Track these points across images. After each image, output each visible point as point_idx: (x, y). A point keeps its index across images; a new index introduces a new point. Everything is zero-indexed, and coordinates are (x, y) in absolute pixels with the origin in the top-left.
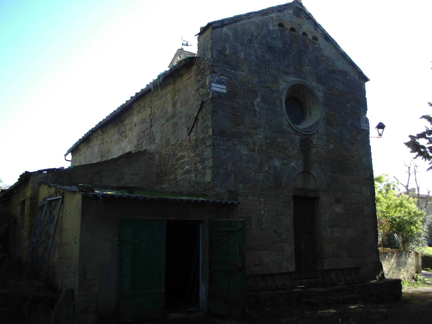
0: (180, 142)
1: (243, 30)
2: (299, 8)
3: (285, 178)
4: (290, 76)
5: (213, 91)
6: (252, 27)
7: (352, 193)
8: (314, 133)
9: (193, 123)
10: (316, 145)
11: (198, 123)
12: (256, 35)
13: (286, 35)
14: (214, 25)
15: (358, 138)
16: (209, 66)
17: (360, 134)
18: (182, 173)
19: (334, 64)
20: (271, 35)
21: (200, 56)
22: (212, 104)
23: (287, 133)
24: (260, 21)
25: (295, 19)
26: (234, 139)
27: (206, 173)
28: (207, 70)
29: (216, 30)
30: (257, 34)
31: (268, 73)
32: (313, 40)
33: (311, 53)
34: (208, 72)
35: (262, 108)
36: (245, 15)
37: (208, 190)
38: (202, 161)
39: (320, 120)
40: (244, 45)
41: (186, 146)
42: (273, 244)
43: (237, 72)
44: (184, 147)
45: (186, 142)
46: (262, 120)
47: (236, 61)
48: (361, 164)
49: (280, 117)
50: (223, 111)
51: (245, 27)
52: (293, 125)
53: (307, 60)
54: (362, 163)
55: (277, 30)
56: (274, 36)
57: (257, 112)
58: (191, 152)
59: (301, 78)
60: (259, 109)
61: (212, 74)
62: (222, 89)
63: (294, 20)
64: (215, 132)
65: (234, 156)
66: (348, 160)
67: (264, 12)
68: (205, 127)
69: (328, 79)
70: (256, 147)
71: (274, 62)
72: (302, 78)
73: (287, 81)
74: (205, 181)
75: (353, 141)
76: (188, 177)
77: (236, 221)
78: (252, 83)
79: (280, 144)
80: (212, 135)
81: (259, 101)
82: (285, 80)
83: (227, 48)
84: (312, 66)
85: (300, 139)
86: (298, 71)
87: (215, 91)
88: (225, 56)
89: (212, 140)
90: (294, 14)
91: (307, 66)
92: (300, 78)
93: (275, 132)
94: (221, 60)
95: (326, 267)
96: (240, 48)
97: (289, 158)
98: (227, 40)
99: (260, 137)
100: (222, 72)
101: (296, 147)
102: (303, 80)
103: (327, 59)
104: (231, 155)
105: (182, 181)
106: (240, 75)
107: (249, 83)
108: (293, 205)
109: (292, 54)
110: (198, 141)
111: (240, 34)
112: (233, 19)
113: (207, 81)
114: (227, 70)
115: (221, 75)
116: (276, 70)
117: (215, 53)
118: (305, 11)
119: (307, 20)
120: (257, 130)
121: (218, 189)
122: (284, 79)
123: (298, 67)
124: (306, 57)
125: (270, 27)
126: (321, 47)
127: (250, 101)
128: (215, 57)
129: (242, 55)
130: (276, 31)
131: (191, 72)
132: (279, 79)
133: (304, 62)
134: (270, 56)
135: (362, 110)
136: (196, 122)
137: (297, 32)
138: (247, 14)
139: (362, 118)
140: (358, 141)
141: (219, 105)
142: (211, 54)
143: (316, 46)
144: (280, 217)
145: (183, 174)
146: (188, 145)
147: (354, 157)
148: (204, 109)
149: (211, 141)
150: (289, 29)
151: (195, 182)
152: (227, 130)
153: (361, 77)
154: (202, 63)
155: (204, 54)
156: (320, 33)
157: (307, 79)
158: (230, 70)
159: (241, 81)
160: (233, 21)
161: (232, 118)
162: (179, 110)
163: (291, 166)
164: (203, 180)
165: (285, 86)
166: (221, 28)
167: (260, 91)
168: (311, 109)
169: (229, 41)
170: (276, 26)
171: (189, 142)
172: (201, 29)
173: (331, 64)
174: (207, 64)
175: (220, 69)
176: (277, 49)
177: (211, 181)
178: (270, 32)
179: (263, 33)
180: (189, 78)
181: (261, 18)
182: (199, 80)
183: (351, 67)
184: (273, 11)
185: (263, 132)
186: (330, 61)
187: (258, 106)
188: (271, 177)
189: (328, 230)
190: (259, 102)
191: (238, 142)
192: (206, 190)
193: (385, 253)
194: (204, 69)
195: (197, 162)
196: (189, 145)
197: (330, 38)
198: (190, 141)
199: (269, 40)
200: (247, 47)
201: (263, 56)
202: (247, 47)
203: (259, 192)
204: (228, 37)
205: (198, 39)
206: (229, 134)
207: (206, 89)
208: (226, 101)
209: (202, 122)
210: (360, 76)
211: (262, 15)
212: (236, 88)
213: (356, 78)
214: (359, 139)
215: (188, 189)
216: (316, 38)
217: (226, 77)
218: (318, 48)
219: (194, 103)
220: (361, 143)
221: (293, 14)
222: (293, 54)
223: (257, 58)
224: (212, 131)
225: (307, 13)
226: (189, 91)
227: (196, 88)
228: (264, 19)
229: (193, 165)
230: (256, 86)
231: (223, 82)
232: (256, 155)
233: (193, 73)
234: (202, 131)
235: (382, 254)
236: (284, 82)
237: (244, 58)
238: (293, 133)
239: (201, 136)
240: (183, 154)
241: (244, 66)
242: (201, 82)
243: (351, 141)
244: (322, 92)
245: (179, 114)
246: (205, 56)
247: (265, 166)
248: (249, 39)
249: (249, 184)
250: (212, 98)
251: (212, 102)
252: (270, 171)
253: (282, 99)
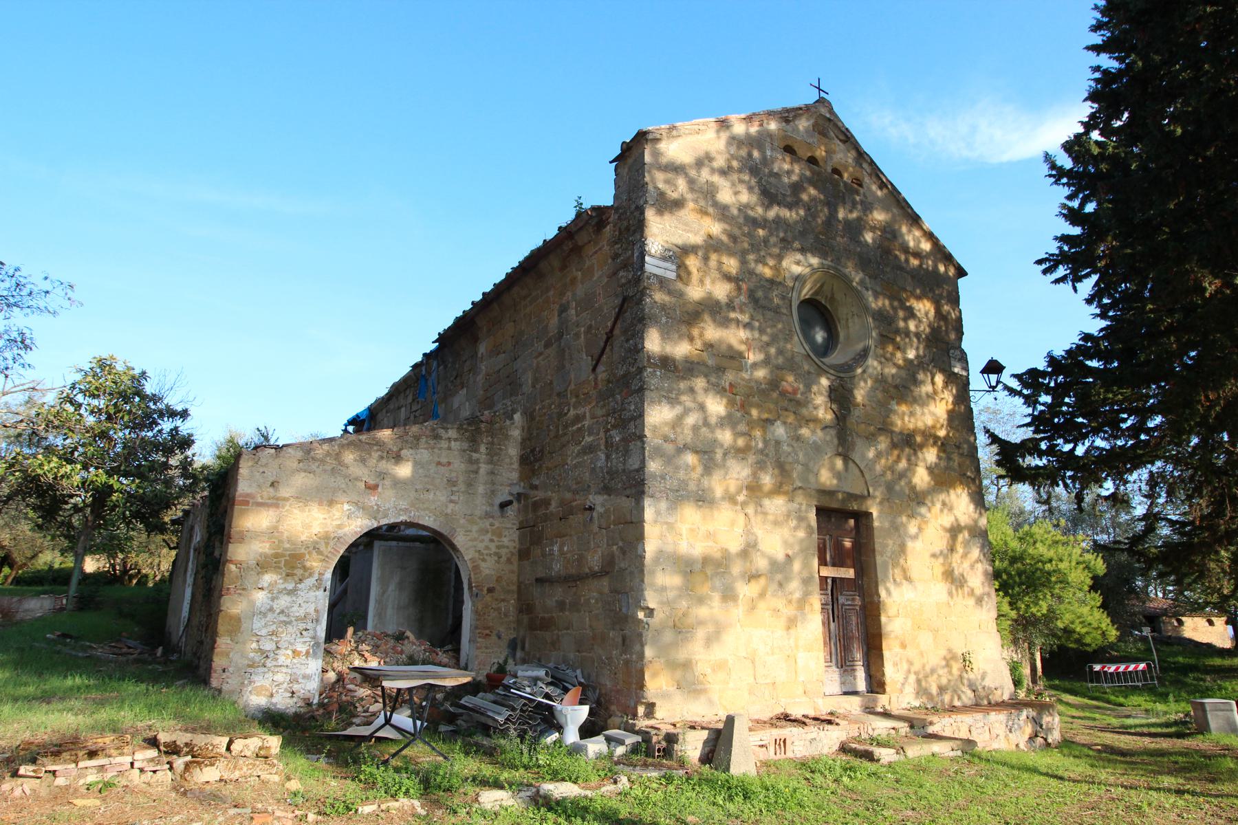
9: (602, 344)
74: (628, 466)
145: (577, 455)
148: (628, 314)
164: (624, 464)
205: (616, 170)
229: (602, 434)
240: (580, 411)
253: (791, 301)
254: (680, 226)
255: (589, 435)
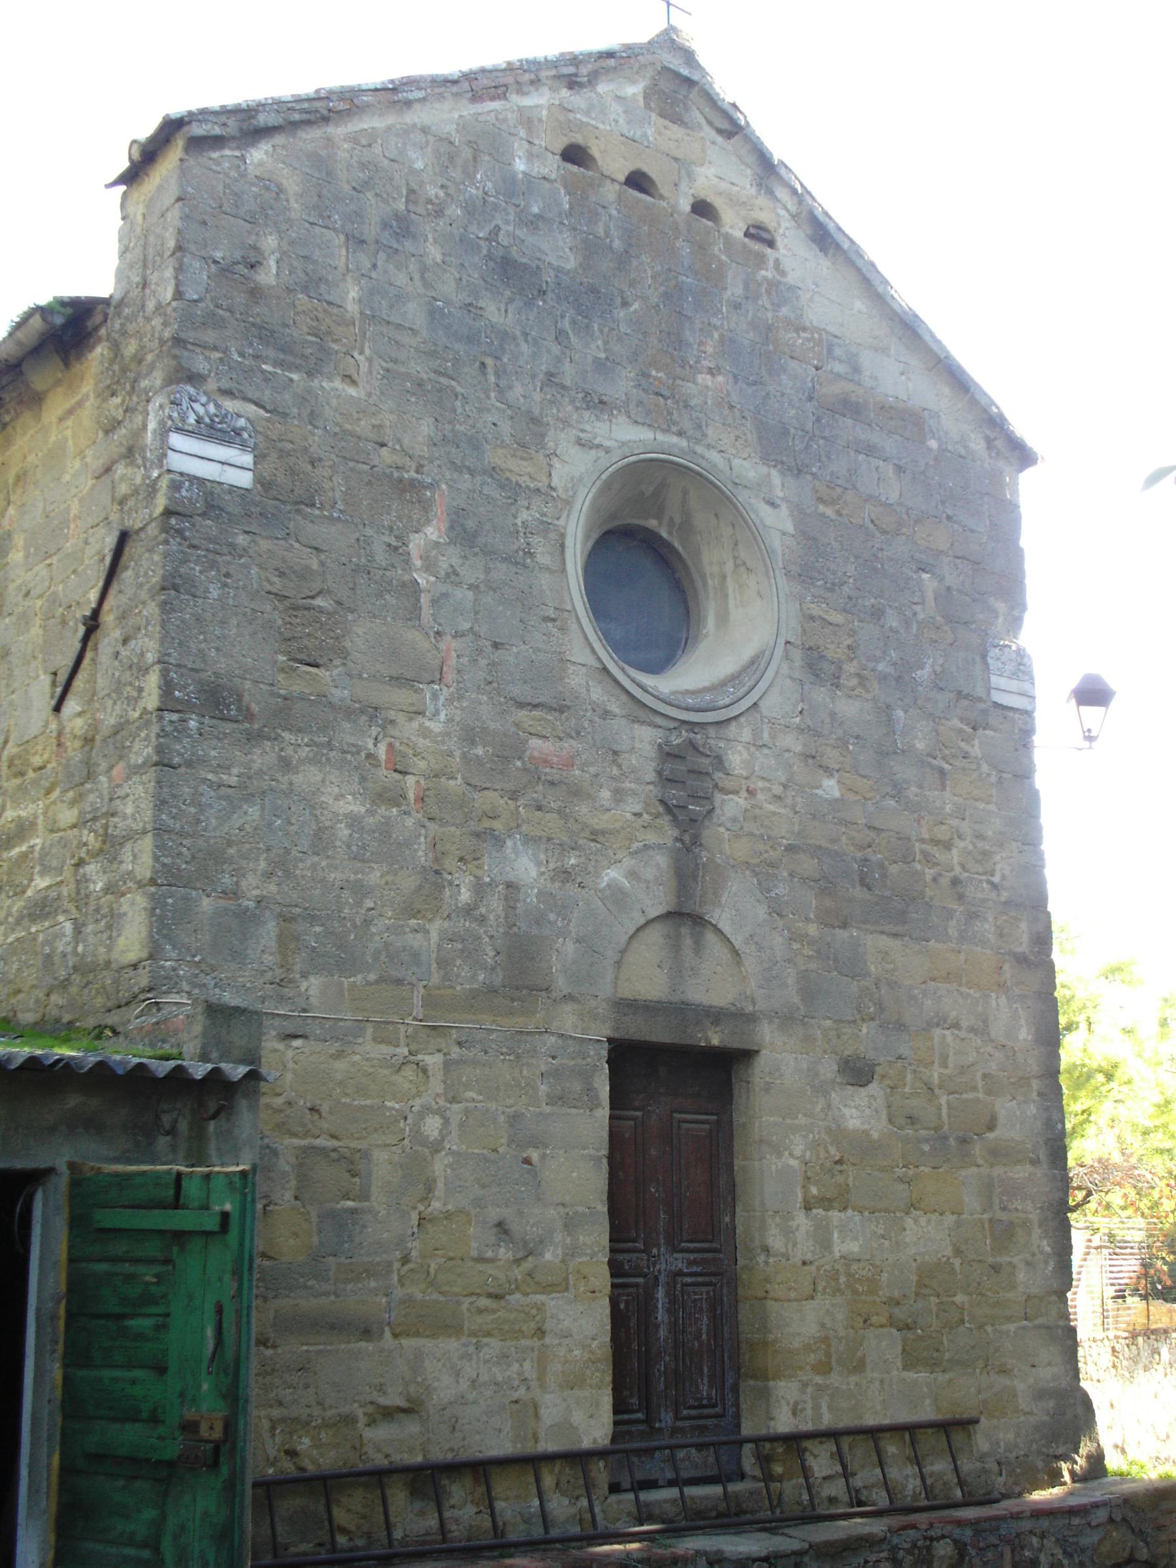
0: (15, 750)
1: (363, 166)
2: (677, 75)
3: (570, 947)
4: (614, 420)
5: (178, 477)
6: (412, 154)
7: (937, 1032)
8: (735, 718)
10: (747, 778)
11: (100, 646)
12: (437, 197)
13: (604, 207)
14: (197, 130)
15: (976, 750)
16: (162, 342)
17: (984, 729)
18: (15, 914)
19: (857, 369)
20: (517, 202)
21: (128, 292)
22: (166, 542)
23: (588, 714)
24: (458, 124)
25: (654, 130)
26: (286, 735)
27: (122, 911)
28: (152, 367)
29: (210, 159)
30: (441, 194)
31: (493, 394)
32: (746, 240)
33: (737, 306)
34: (155, 374)
35: (452, 575)
36: (376, 90)
37: (127, 1004)
38: (107, 847)
39: (767, 653)
40: (363, 242)
41: (41, 768)
42: (490, 1296)
43: (316, 381)
44: (31, 774)
45: (40, 748)
46: (449, 638)
47: (315, 324)
48: (985, 885)
49: (550, 625)
50: (225, 585)
51: (377, 149)
52: (623, 670)
53: (711, 343)
54: (992, 879)
55: (553, 176)
56: (535, 210)
57: (424, 600)
58: (62, 801)
59: (674, 429)
60: (433, 579)
61: (178, 384)
62: (226, 468)
63: (650, 131)
64: (177, 693)
65: (279, 822)
66: (919, 862)
67: (485, 81)
68: (130, 667)
69: (821, 442)
70: (410, 780)
71: (526, 341)
72: (680, 434)
73: (597, 441)
74: (115, 956)
75: (947, 762)
76: (41, 937)
77: (207, 1177)
78: (399, 441)
79: (548, 770)
80: (160, 710)
81: (434, 537)
82: (582, 435)
83: (266, 254)
84: (735, 376)
85: (660, 745)
86: (657, 394)
87: (188, 475)
88: (256, 293)
89: (158, 736)
90: (653, 105)
91: (711, 372)
92: (667, 431)
93: (521, 705)
94: (228, 314)
95: (784, 1423)
96: (343, 259)
97: (594, 840)
98: (270, 212)
99: (436, 727)
100: (234, 376)
101: (633, 786)
102: (684, 443)
103: (821, 340)
104: (262, 817)
105: (15, 959)
106: (334, 402)
107: (383, 445)
108: (608, 1088)
109: (632, 309)
110: (98, 743)
111: (346, 188)
112: (306, 105)
113: (152, 425)
114: (264, 366)
115: (228, 393)
116: (539, 384)
117: (200, 278)
118: (711, 92)
119: (720, 140)
120: (417, 691)
121: (182, 997)
122: (583, 431)
123: (659, 375)
124: (709, 324)
125: (517, 160)
126: (791, 279)
127: (387, 539)
128: (195, 297)
129: (353, 293)
130: (547, 185)
131: (82, 379)
132: (553, 431)
133: (695, 353)
134: (506, 311)
135: (1001, 607)
136: (90, 644)
137: (662, 197)
138: (391, 86)
139: (997, 650)
140: (974, 766)
141: (207, 550)
142: (176, 278)
143: (763, 272)
144: (535, 1156)
145: (18, 922)
146: (49, 766)
147: (947, 846)
148: (129, 573)
149: (153, 739)
150: (622, 178)
151: (71, 964)
152: (248, 685)
153: (999, 444)
154: (131, 328)
155: (145, 285)
156: (788, 211)
157: (704, 435)
158: (279, 371)
159: (337, 429)
160: (309, 112)
161: (280, 622)
162: (19, 582)
163: (603, 885)
164: (110, 949)
165: (583, 470)
166: (238, 148)
167: (444, 487)
168: (726, 596)
169: (281, 218)
170: (550, 155)
171: (55, 748)
172: (133, 151)
173: (840, 368)
174: (153, 336)
175: (221, 359)
176: (548, 277)
177: (144, 954)
178: (511, 187)
179: (474, 191)
180: (70, 412)
181: (465, 113)
182: (114, 418)
183: (946, 390)
184: (532, 76)
185: (450, 701)
186: (838, 352)
187: (430, 566)
188: (492, 937)
189: (801, 1221)
190: (437, 544)
191: (308, 749)
192: (119, 1007)
193: (1154, 1332)
194: (139, 359)
195: (88, 851)
196: (54, 764)
197: (839, 238)
198: (59, 745)
199: (504, 228)
200: (382, 256)
201: (470, 304)
202: (382, 256)
203: (415, 1019)
204: (277, 199)
205: (123, 206)
206: (255, 708)
207: (145, 467)
208: (247, 529)
209: (116, 640)
210: (996, 438)
211: (470, 95)
212: (310, 467)
213: (972, 445)
214: (980, 756)
215: (37, 1001)
216: (766, 236)
217: (254, 407)
218: (773, 285)
219: (86, 542)
220: (988, 775)
221: (647, 106)
222: (636, 306)
223: (434, 314)
224: (160, 688)
225: (720, 103)
226: (67, 478)
227: (101, 461)
228: (481, 119)
229: (68, 872)
230: (425, 462)
231: (238, 432)
232: (410, 822)
233: (92, 382)
234: (114, 691)
235: (1140, 1340)
236: (577, 447)
237: (361, 313)
238: (617, 711)
239: (111, 715)
241: (361, 352)
242: (124, 431)
243: (935, 762)
244: (784, 510)
245: (16, 604)
246: (147, 291)
247: (457, 882)
248: (397, 216)
249: (360, 977)
250: (168, 513)
251: (167, 533)
252: (483, 910)
253: (563, 536)
254: (271, 353)
255: (42, 874)
